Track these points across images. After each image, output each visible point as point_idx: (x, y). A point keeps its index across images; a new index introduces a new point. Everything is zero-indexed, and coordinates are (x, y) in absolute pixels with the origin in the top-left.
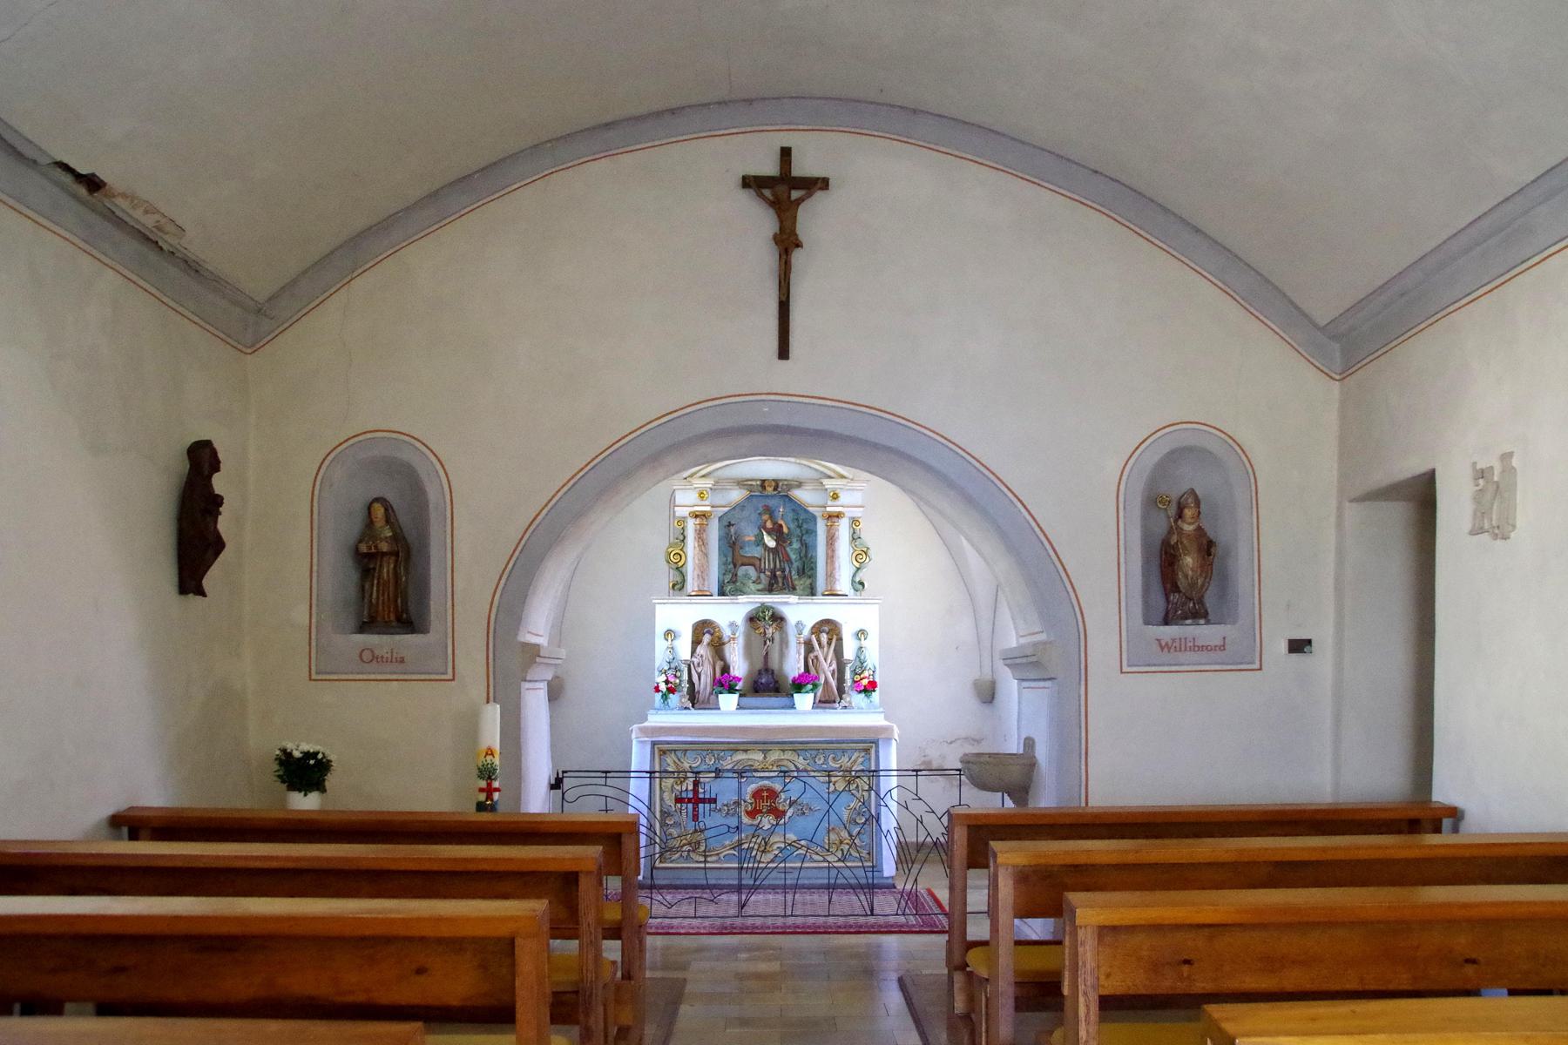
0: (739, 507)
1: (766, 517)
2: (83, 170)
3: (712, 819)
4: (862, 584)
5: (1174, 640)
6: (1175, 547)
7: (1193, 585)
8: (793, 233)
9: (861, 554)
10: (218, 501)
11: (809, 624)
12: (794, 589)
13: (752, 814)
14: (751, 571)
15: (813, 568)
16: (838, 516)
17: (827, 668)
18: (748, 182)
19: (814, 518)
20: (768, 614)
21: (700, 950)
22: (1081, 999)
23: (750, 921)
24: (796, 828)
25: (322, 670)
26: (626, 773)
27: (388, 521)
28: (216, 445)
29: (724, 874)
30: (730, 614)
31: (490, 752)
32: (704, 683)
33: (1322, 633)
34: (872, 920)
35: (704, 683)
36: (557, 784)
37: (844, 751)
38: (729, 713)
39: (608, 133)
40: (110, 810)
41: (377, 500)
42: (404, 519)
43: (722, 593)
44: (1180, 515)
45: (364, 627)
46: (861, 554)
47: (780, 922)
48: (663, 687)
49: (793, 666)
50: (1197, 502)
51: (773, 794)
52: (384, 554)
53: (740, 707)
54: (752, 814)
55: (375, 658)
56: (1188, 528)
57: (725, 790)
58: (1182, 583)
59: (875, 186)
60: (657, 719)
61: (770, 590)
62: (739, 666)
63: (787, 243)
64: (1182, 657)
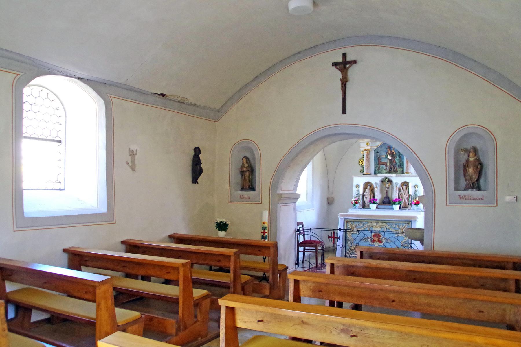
1: (388, 150)
11: (400, 183)
14: (384, 166)
15: (403, 165)
17: (405, 197)
18: (335, 64)
20: (387, 180)
25: (232, 200)
30: (376, 180)
31: (264, 223)
32: (367, 201)
35: (367, 201)
37: (401, 224)
38: (373, 211)
39: (298, 55)
41: (244, 157)
43: (375, 173)
45: (243, 189)
48: (353, 202)
49: (395, 196)
53: (377, 208)
59: (370, 61)
61: (390, 172)
62: (378, 196)
63: (344, 82)
64: (467, 201)
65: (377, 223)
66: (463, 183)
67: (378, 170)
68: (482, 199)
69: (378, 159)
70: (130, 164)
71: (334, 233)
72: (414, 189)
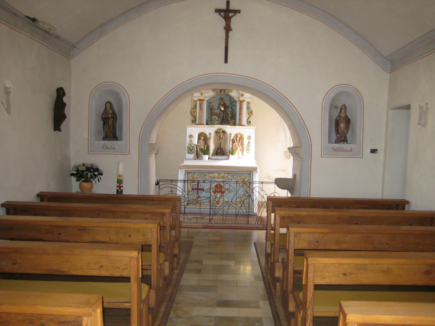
0: (213, 97)
1: (221, 101)
2: (32, 17)
3: (203, 194)
4: (250, 122)
5: (337, 148)
6: (338, 121)
7: (343, 132)
8: (230, 27)
9: (250, 113)
10: (65, 105)
12: (229, 123)
13: (215, 192)
14: (216, 117)
16: (244, 101)
18: (218, 11)
19: (236, 102)
21: (198, 233)
22: (290, 250)
23: (212, 225)
24: (228, 197)
26: (177, 181)
27: (111, 108)
28: (64, 88)
29: (206, 210)
30: (210, 130)
33: (381, 148)
34: (248, 225)
36: (157, 184)
37: (243, 174)
40: (37, 192)
42: (115, 107)
44: (341, 112)
45: (105, 138)
46: (250, 113)
47: (221, 225)
50: (346, 108)
51: (221, 187)
52: (109, 118)
54: (215, 192)
55: (107, 148)
56: (343, 115)
57: (206, 186)
58: (340, 131)
60: (186, 163)
61: (222, 123)
63: (228, 29)
65: (219, 174)
66: (334, 137)
67: (211, 120)
68: (351, 151)
69: (210, 109)
70: (5, 105)
71: (198, 185)
72: (189, 139)
